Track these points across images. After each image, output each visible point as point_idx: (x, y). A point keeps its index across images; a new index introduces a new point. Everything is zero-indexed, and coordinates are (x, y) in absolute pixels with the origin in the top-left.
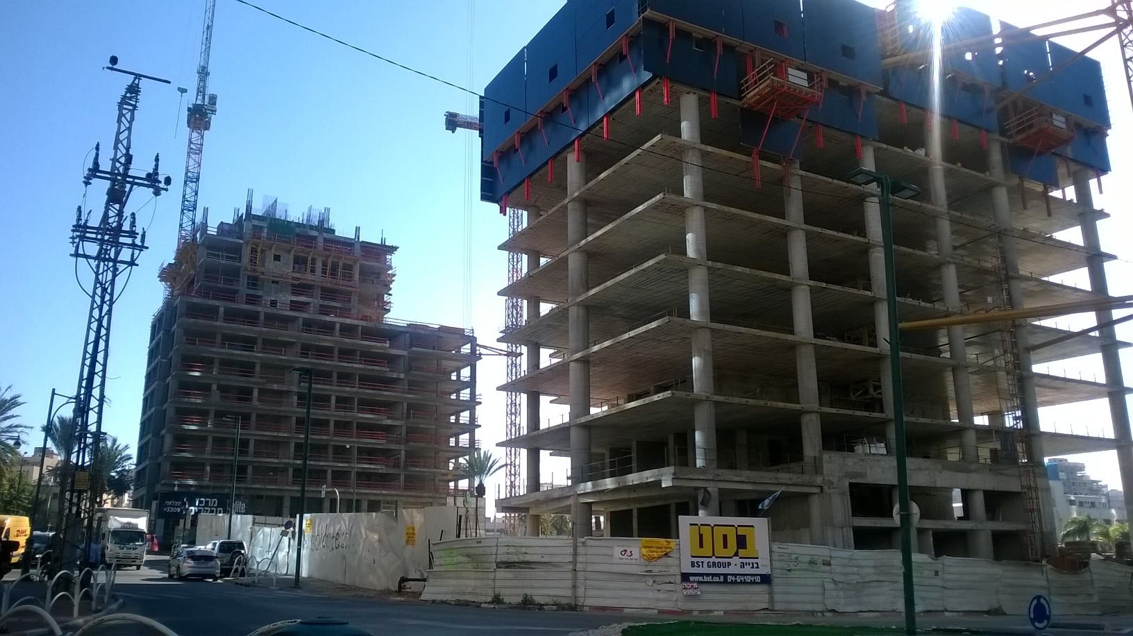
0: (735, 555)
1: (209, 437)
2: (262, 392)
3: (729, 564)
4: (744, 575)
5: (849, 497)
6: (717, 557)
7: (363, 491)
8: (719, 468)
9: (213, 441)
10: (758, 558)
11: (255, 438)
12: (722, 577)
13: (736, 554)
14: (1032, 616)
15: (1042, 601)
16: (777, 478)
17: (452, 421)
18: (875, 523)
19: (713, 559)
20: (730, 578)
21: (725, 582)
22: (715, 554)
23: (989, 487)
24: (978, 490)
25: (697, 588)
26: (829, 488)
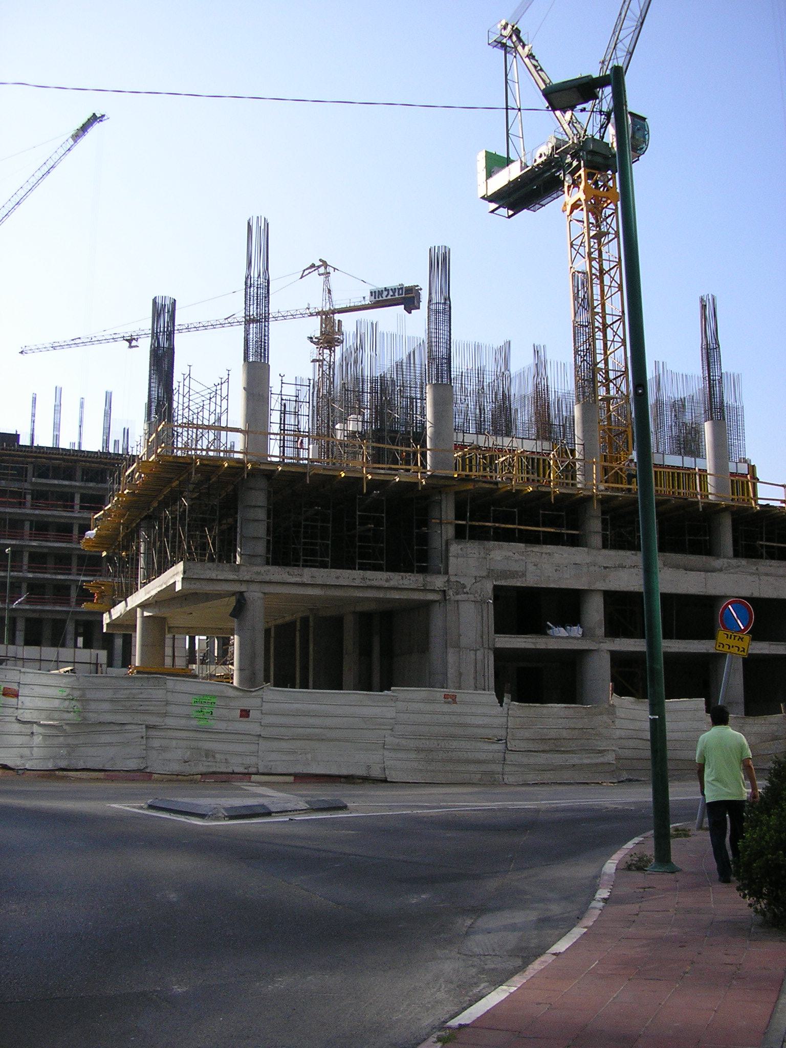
1: (76, 495)
5: (491, 607)
11: (78, 552)
16: (363, 579)
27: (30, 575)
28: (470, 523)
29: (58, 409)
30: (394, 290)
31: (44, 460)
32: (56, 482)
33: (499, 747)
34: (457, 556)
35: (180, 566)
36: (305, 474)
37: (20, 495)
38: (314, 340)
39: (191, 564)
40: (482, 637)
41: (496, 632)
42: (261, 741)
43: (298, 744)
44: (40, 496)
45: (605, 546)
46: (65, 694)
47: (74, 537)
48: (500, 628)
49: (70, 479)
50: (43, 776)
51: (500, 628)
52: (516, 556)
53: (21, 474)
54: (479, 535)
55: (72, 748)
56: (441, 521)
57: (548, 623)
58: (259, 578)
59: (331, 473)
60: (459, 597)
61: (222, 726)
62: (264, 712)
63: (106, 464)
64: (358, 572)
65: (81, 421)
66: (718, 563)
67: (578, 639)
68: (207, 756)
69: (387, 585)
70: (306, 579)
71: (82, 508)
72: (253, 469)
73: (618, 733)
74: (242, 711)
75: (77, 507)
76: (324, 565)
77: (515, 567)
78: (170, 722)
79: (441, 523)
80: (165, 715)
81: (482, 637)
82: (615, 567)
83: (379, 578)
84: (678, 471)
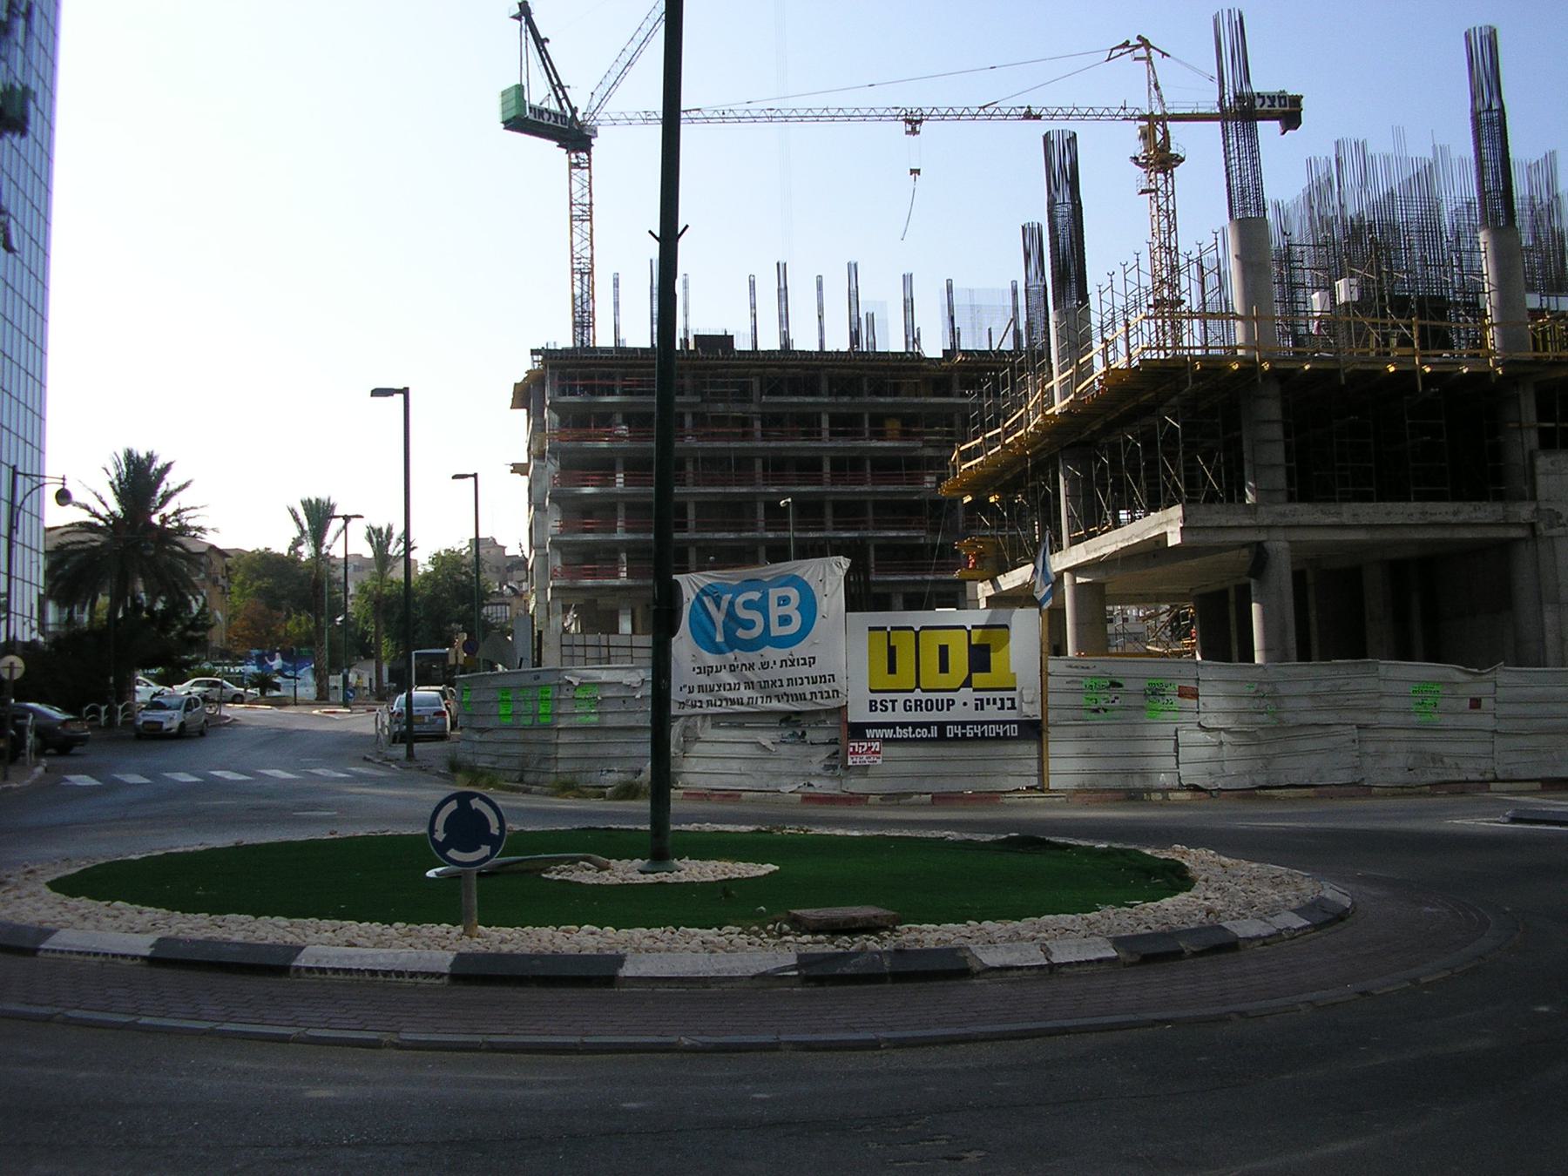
0: (961, 686)
2: (700, 419)
3: (951, 702)
4: (982, 723)
6: (923, 691)
7: (892, 578)
8: (1291, 499)
9: (766, 509)
10: (1014, 689)
11: (832, 498)
12: (934, 729)
13: (967, 683)
16: (1424, 513)
19: (918, 695)
21: (942, 737)
25: (879, 753)
26: (1551, 526)
27: (771, 535)
28: (1561, 425)
29: (783, 294)
30: (1272, 98)
31: (775, 369)
32: (795, 399)
34: (1547, 473)
35: (1176, 511)
36: (1338, 371)
37: (745, 422)
38: (1141, 160)
39: (1192, 507)
43: (1543, 739)
44: (774, 422)
46: (1252, 690)
47: (825, 476)
49: (813, 394)
50: (1244, 797)
53: (744, 394)
58: (1285, 521)
60: (1555, 532)
61: (1449, 721)
62: (1498, 700)
63: (861, 368)
64: (1415, 504)
65: (821, 308)
68: (1434, 760)
69: (1454, 520)
71: (832, 434)
72: (1271, 369)
74: (1472, 700)
75: (826, 434)
78: (1384, 718)
79: (1520, 428)
80: (1377, 711)
83: (1443, 510)
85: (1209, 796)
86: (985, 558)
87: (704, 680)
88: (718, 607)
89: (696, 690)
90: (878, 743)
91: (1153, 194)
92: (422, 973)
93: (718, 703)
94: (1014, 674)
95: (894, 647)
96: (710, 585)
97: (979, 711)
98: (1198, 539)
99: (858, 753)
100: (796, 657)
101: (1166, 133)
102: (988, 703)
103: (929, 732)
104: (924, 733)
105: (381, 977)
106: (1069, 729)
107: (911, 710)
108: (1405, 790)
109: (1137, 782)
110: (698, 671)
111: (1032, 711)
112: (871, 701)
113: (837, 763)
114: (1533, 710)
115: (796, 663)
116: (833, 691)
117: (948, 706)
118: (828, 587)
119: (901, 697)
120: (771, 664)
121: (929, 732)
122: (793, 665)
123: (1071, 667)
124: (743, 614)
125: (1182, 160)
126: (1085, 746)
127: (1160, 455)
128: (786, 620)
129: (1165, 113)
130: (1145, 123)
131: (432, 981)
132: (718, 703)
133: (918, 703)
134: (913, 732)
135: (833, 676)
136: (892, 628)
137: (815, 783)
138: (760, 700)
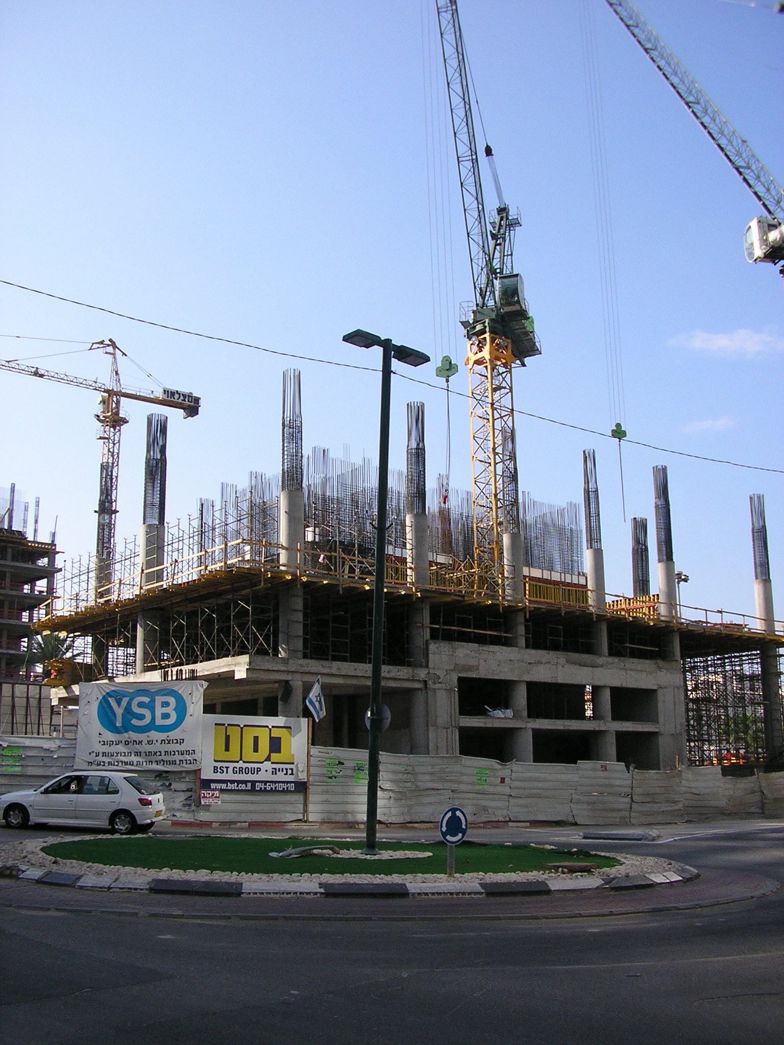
0: (265, 760)
3: (259, 770)
5: (457, 694)
6: (244, 762)
8: (305, 656)
10: (293, 763)
12: (249, 785)
14: (444, 829)
15: (458, 813)
17: (25, 591)
18: (485, 723)
19: (241, 764)
20: (258, 786)
21: (253, 790)
22: (243, 759)
23: (617, 683)
24: (605, 687)
25: (218, 797)
28: (442, 627)
30: (184, 396)
33: (628, 800)
34: (434, 653)
35: (245, 658)
40: (451, 718)
41: (461, 714)
42: (511, 800)
45: (527, 647)
48: (463, 711)
50: (402, 827)
51: (463, 711)
52: (473, 654)
54: (449, 637)
55: (410, 807)
56: (423, 625)
57: (486, 706)
59: (731, 633)
60: (436, 686)
66: (601, 660)
67: (511, 719)
70: (334, 671)
73: (684, 789)
76: (344, 659)
77: (473, 662)
78: (462, 787)
81: (451, 718)
82: (536, 663)
84: (569, 588)
85: (385, 826)
86: (64, 673)
87: (106, 749)
88: (119, 704)
89: (101, 755)
90: (217, 792)
91: (107, 441)
92: (473, 893)
93: (116, 764)
94: (293, 755)
95: (229, 736)
96: (113, 691)
97: (274, 775)
98: (255, 676)
99: (206, 797)
100: (171, 739)
101: (118, 403)
102: (279, 771)
103: (246, 786)
104: (243, 787)
105: (455, 896)
106: (319, 787)
107: (236, 773)
108: (473, 825)
109: (350, 818)
110: (103, 743)
111: (303, 777)
112: (214, 767)
113: (193, 802)
114: (526, 785)
115: (171, 742)
116: (193, 760)
117: (258, 771)
118: (194, 699)
119: (232, 765)
120: (155, 742)
121: (246, 786)
122: (169, 743)
123: (320, 752)
124: (136, 710)
125: (127, 422)
126: (324, 797)
127: (232, 623)
128: (166, 716)
129: (120, 391)
130: (106, 395)
131: (479, 896)
132: (116, 764)
133: (241, 769)
134: (237, 786)
135: (194, 751)
136: (228, 725)
137: (178, 814)
138: (145, 763)
